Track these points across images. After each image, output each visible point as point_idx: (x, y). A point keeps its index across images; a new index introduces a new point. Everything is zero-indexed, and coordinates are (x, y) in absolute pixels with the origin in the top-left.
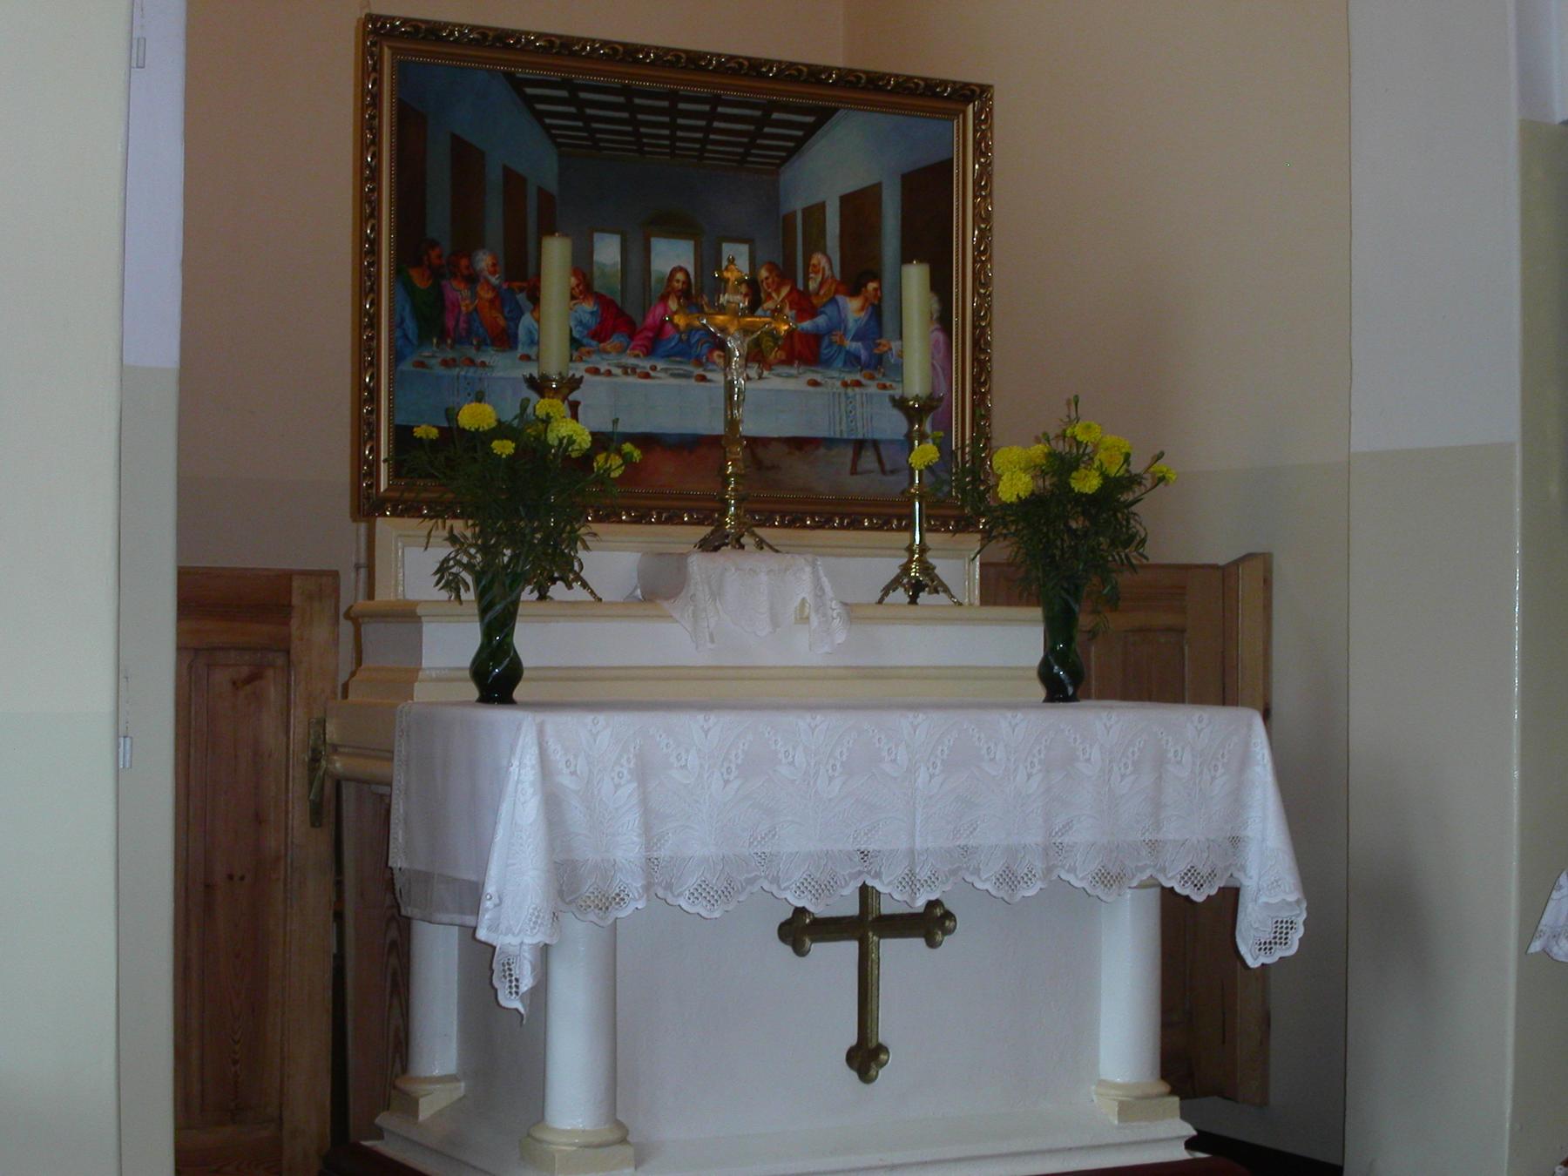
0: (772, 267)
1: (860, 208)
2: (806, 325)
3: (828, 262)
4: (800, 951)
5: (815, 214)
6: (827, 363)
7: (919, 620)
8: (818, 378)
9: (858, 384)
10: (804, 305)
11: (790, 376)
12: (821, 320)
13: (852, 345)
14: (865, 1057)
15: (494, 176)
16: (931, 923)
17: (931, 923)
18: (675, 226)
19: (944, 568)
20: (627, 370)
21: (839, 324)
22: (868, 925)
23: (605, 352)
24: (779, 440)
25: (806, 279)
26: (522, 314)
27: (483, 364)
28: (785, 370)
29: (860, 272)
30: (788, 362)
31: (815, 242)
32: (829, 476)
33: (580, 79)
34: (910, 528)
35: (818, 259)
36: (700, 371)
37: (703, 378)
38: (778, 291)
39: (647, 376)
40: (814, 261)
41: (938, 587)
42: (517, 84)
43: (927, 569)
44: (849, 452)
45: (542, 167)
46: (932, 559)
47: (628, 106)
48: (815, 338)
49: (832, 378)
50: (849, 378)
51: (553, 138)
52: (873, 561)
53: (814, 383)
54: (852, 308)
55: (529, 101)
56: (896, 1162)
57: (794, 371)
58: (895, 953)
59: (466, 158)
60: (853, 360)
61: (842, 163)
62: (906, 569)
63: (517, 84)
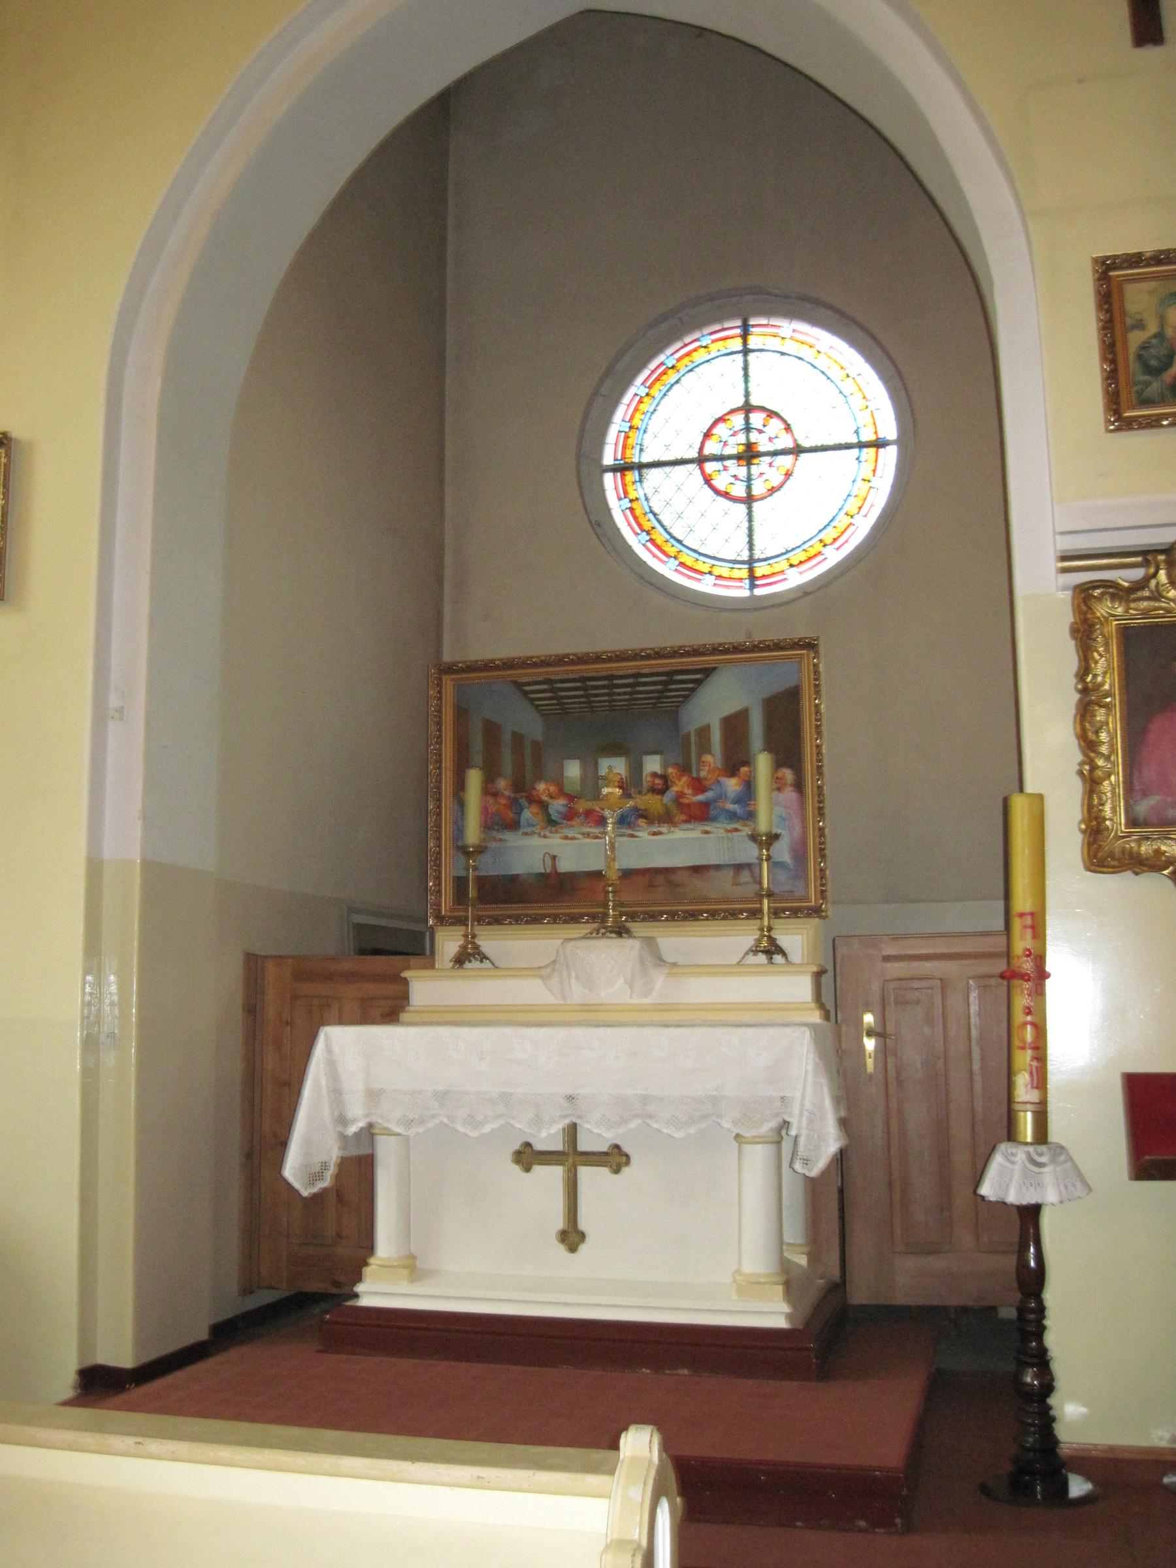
0: (676, 765)
1: (735, 725)
2: (700, 798)
3: (714, 759)
4: (528, 1169)
5: (704, 732)
6: (714, 819)
7: (775, 973)
8: (708, 828)
9: (736, 830)
10: (699, 786)
11: (688, 830)
12: (709, 795)
13: (731, 807)
14: (572, 1237)
15: (507, 737)
16: (615, 1158)
17: (615, 1158)
18: (614, 750)
19: (783, 940)
20: (588, 835)
21: (722, 796)
22: (571, 1156)
23: (572, 826)
24: (682, 868)
25: (698, 771)
26: (522, 809)
27: (501, 840)
28: (687, 826)
29: (736, 761)
30: (687, 821)
31: (705, 747)
32: (723, 884)
33: (553, 677)
34: (761, 919)
35: (708, 758)
36: (630, 832)
37: (632, 836)
38: (679, 779)
39: (597, 837)
40: (703, 759)
41: (781, 951)
42: (518, 685)
43: (772, 941)
44: (731, 872)
45: (532, 725)
46: (774, 934)
47: (553, 690)
48: (706, 804)
49: (718, 829)
50: (729, 827)
51: (539, 711)
52: (740, 938)
53: (707, 832)
54: (732, 785)
55: (526, 693)
56: (569, 1301)
57: (691, 826)
58: (586, 1174)
59: (492, 731)
60: (733, 816)
61: (724, 697)
62: (759, 941)
63: (518, 685)
